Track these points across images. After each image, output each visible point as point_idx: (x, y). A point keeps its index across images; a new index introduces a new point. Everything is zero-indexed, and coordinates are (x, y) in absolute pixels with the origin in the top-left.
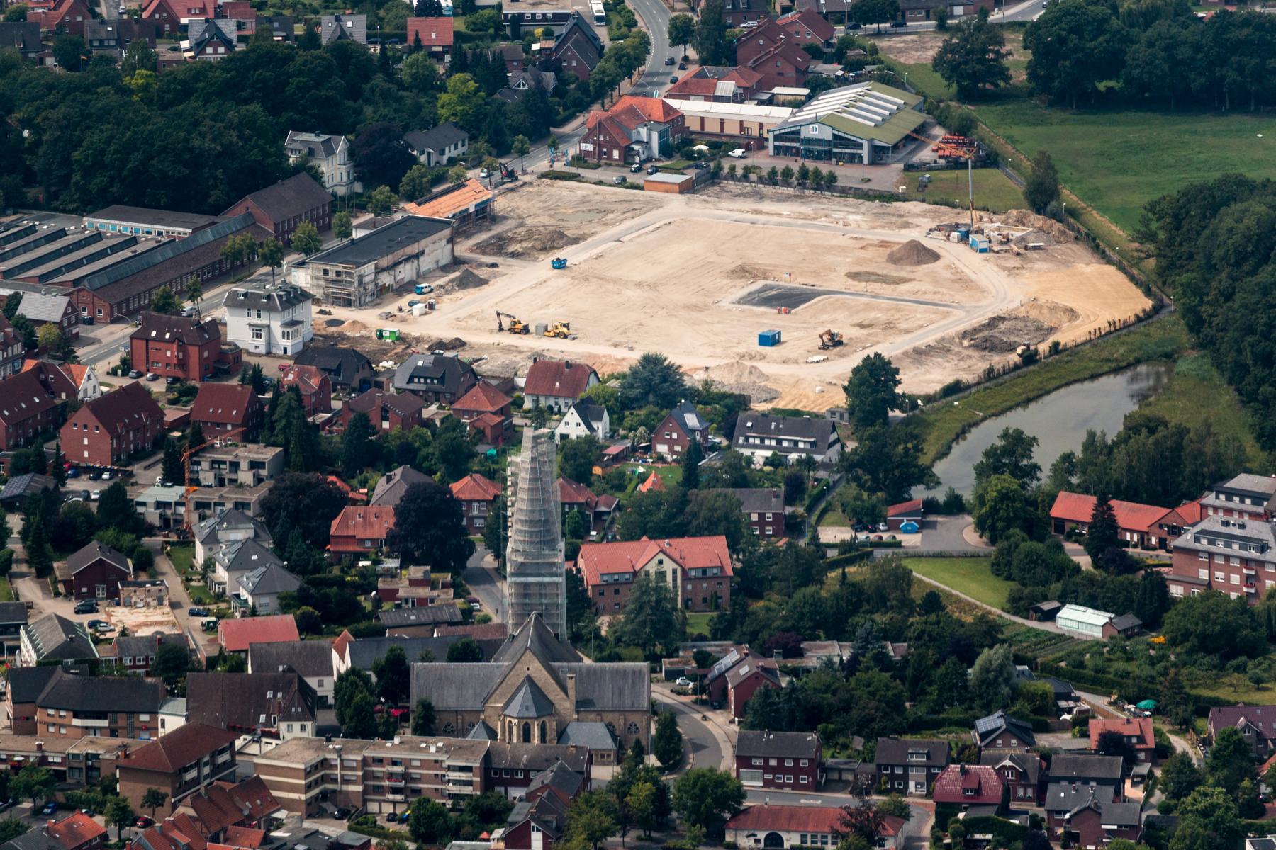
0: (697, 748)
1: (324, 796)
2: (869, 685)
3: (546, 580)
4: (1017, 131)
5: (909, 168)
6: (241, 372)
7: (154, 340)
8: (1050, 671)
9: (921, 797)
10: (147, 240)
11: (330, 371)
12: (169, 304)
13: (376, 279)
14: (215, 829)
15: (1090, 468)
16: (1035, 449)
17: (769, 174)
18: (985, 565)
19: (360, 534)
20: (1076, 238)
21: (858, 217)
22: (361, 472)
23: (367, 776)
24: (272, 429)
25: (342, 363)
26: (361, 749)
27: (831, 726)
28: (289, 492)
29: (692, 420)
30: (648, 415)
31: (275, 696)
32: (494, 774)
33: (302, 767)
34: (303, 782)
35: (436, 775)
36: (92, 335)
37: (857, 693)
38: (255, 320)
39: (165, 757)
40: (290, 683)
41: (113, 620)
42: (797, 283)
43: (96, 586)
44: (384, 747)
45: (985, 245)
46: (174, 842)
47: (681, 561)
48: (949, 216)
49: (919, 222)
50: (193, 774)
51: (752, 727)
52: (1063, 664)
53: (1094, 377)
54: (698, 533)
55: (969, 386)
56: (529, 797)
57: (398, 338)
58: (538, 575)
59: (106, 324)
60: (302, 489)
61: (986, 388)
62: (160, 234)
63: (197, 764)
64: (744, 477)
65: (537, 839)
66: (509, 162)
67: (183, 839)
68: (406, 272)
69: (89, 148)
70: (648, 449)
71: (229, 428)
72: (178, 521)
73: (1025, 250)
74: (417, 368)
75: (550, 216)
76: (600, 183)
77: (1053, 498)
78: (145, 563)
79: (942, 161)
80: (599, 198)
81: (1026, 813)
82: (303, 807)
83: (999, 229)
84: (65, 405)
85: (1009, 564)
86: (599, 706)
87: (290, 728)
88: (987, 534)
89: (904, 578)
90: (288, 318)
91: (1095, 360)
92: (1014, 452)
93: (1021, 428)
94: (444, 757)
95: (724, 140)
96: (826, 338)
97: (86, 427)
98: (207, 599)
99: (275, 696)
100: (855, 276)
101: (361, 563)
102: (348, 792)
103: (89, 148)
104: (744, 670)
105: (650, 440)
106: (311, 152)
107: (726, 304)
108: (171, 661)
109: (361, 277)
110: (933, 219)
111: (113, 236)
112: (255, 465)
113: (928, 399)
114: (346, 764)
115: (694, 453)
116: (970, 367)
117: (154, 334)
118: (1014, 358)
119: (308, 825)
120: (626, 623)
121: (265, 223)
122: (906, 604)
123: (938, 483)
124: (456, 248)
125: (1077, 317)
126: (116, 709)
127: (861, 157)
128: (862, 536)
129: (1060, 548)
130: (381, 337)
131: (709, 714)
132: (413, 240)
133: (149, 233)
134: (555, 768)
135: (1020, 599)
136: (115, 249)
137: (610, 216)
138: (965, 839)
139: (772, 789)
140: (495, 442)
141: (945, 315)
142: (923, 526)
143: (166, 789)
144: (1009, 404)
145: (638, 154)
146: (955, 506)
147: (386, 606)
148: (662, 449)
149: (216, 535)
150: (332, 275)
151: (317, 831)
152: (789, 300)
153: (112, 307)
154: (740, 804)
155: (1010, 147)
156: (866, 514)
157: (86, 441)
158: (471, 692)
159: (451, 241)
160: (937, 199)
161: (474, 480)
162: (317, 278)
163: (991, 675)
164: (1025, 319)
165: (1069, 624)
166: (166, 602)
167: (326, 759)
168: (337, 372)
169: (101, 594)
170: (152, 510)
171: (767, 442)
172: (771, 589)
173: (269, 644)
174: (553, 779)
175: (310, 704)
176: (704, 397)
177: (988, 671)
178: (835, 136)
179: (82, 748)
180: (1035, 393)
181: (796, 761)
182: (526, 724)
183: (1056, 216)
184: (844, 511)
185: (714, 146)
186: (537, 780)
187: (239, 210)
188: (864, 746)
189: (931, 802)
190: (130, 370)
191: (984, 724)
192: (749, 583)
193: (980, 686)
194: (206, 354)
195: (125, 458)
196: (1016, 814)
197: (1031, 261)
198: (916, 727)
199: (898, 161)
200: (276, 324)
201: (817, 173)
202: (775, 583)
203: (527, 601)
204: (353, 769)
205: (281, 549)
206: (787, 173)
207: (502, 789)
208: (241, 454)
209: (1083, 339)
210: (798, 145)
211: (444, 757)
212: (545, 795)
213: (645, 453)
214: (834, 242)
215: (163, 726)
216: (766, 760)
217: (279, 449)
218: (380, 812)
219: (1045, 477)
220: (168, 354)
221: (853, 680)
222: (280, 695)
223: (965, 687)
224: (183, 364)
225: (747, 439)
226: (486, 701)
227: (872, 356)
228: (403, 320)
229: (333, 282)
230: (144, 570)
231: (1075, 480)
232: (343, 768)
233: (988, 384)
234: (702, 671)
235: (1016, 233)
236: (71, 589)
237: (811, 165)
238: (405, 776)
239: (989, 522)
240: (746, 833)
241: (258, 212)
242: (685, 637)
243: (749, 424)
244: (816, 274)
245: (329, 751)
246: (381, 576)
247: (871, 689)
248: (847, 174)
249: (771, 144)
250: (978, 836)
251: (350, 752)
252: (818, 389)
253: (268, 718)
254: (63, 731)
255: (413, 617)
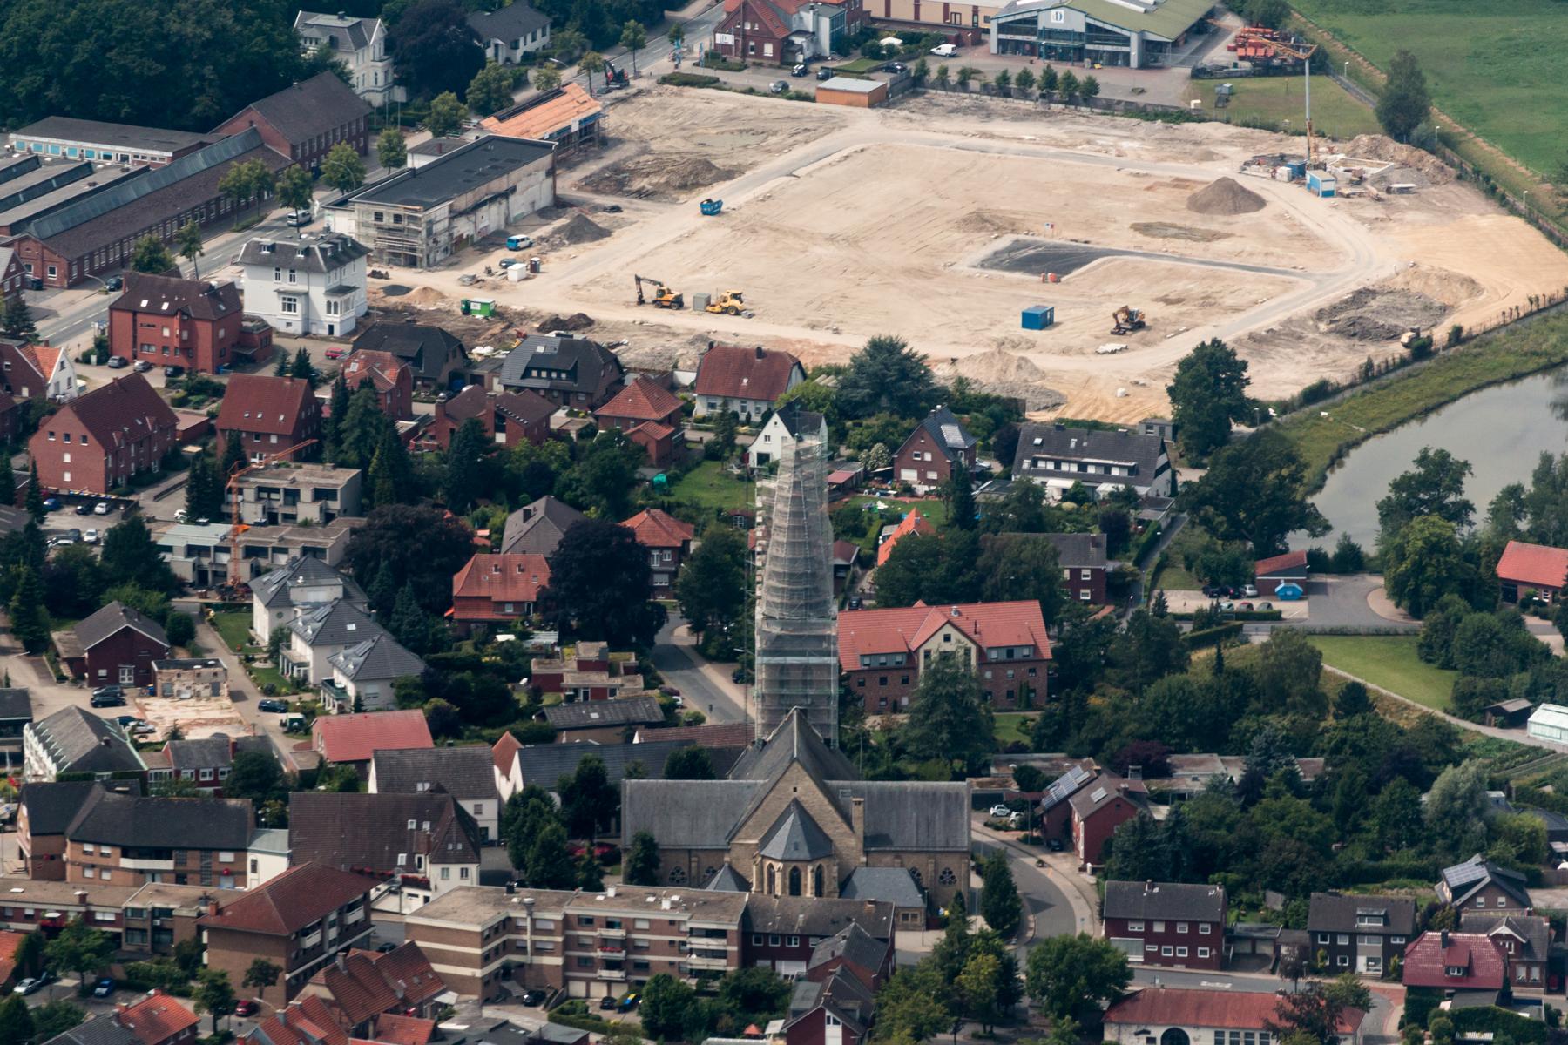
0: (1039, 906)
1: (506, 972)
2: (1282, 818)
3: (814, 660)
4: (1345, 22)
5: (1198, 73)
6: (279, 360)
7: (146, 312)
8: (1527, 798)
9: (1376, 979)
10: (106, 167)
11: (407, 359)
12: (159, 261)
13: (450, 228)
14: (361, 1017)
15: (1548, 507)
16: (1467, 479)
17: (998, 81)
18: (1409, 647)
19: (498, 596)
20: (1459, 178)
21: (1136, 144)
22: (475, 507)
23: (570, 943)
24: (338, 442)
25: (432, 351)
26: (560, 903)
27: (1233, 876)
28: (390, 533)
29: (952, 434)
30: (884, 427)
31: (419, 827)
32: (756, 941)
33: (478, 929)
34: (478, 951)
35: (672, 943)
36: (43, 305)
37: (1267, 828)
38: (286, 285)
39: (275, 912)
40: (441, 808)
41: (150, 716)
42: (1063, 237)
43: (120, 666)
44: (594, 902)
45: (1330, 186)
46: (302, 1036)
47: (975, 637)
48: (1269, 144)
49: (1225, 153)
50: (311, 940)
51: (1123, 875)
52: (1548, 789)
53: (1516, 377)
54: (994, 598)
55: (1338, 390)
56: (813, 975)
57: (494, 313)
58: (802, 654)
59: (62, 288)
60: (406, 531)
61: (1365, 392)
62: (125, 159)
63: (319, 924)
64: (1040, 517)
65: (834, 1037)
66: (618, 60)
67: (316, 1032)
68: (491, 218)
69: (13, 34)
70: (888, 476)
71: (274, 440)
72: (221, 575)
73: (1388, 191)
74: (536, 356)
75: (684, 138)
76: (751, 91)
77: (1498, 551)
78: (182, 633)
79: (1246, 65)
80: (751, 113)
81: (1539, 1002)
82: (479, 987)
83: (1343, 163)
84: (27, 405)
85: (1446, 644)
86: (898, 845)
87: (445, 874)
88: (1406, 603)
89: (1310, 664)
90: (334, 283)
91: (1515, 353)
92: (1436, 480)
93: (1448, 449)
94: (684, 917)
95: (924, 30)
96: (1121, 317)
97: (67, 437)
98: (279, 684)
99: (419, 827)
100: (1145, 229)
101: (501, 638)
102: (541, 966)
103: (13, 34)
104: (1099, 794)
105: (891, 464)
106: (333, 42)
107: (963, 267)
108: (253, 777)
109: (431, 223)
110: (1245, 148)
111: (55, 162)
112: (321, 494)
113: (1284, 407)
114: (539, 925)
115: (960, 482)
116: (1341, 363)
117: (144, 303)
118: (1397, 349)
119: (489, 1012)
120: (912, 725)
121: (277, 145)
122: (1316, 701)
123: (1328, 528)
124: (559, 183)
125: (1480, 291)
126: (185, 844)
127: (1127, 55)
128: (1224, 603)
129: (1520, 623)
130: (467, 310)
131: (1047, 858)
132: (501, 170)
133: (107, 157)
134: (847, 932)
135: (1473, 695)
136: (64, 179)
137: (773, 140)
138: (1453, 1039)
139: (1157, 966)
140: (662, 463)
141: (1287, 287)
142: (1309, 590)
143: (278, 961)
144: (1399, 415)
145: (801, 50)
146: (1350, 561)
147: (548, 699)
148: (909, 475)
149: (288, 595)
150: (388, 221)
151: (506, 1023)
152: (1055, 262)
153: (70, 265)
154: (1123, 986)
155: (1340, 46)
156: (1225, 572)
157: (67, 458)
158: (710, 822)
159: (551, 173)
160: (1248, 118)
161: (653, 518)
162: (366, 225)
163: (1458, 804)
164: (1405, 293)
165: (1547, 731)
166: (224, 691)
167: (509, 919)
168: (417, 360)
169: (126, 678)
170: (181, 558)
171: (1065, 467)
172: (1103, 678)
173: (401, 751)
174: (848, 949)
175: (472, 841)
176: (962, 402)
177: (1453, 799)
178: (1089, 26)
179: (146, 899)
180: (1435, 400)
181: (1194, 925)
182: (795, 869)
183: (1421, 144)
184: (1189, 568)
185: (909, 39)
186: (822, 952)
187: (239, 126)
188: (1285, 905)
189: (1400, 986)
190: (109, 356)
191: (1458, 874)
192: (1073, 670)
193: (1441, 820)
194: (222, 333)
195: (129, 481)
196: (1525, 1003)
197: (1399, 210)
198: (1356, 877)
199: (1182, 63)
200: (318, 294)
201: (1069, 80)
202: (1109, 672)
203: (785, 691)
204: (549, 932)
205: (384, 611)
206: (1025, 79)
207: (768, 963)
208: (300, 479)
209: (1494, 322)
210: (1034, 39)
211: (684, 917)
212: (838, 969)
213: (884, 482)
214: (1106, 180)
215: (254, 869)
216: (1149, 924)
217: (355, 472)
218: (588, 996)
219: (1480, 523)
220: (166, 332)
221: (1256, 812)
222: (426, 826)
223: (1418, 821)
224: (187, 348)
225: (1035, 462)
226: (732, 836)
227: (1208, 343)
228: (496, 288)
229: (390, 230)
230: (182, 644)
231: (1523, 525)
232: (535, 931)
233: (1366, 386)
234: (1029, 797)
235: (1372, 171)
236: (80, 671)
237: (1061, 69)
238: (625, 944)
239: (1411, 584)
240: (1134, 1029)
241: (267, 129)
242: (995, 746)
243: (1038, 441)
244: (1088, 225)
245: (514, 907)
246: (534, 655)
247: (1286, 823)
248: (1114, 83)
249: (993, 38)
250: (1472, 1036)
251: (544, 908)
252: (1120, 391)
253: (410, 859)
254: (106, 876)
255: (595, 716)
